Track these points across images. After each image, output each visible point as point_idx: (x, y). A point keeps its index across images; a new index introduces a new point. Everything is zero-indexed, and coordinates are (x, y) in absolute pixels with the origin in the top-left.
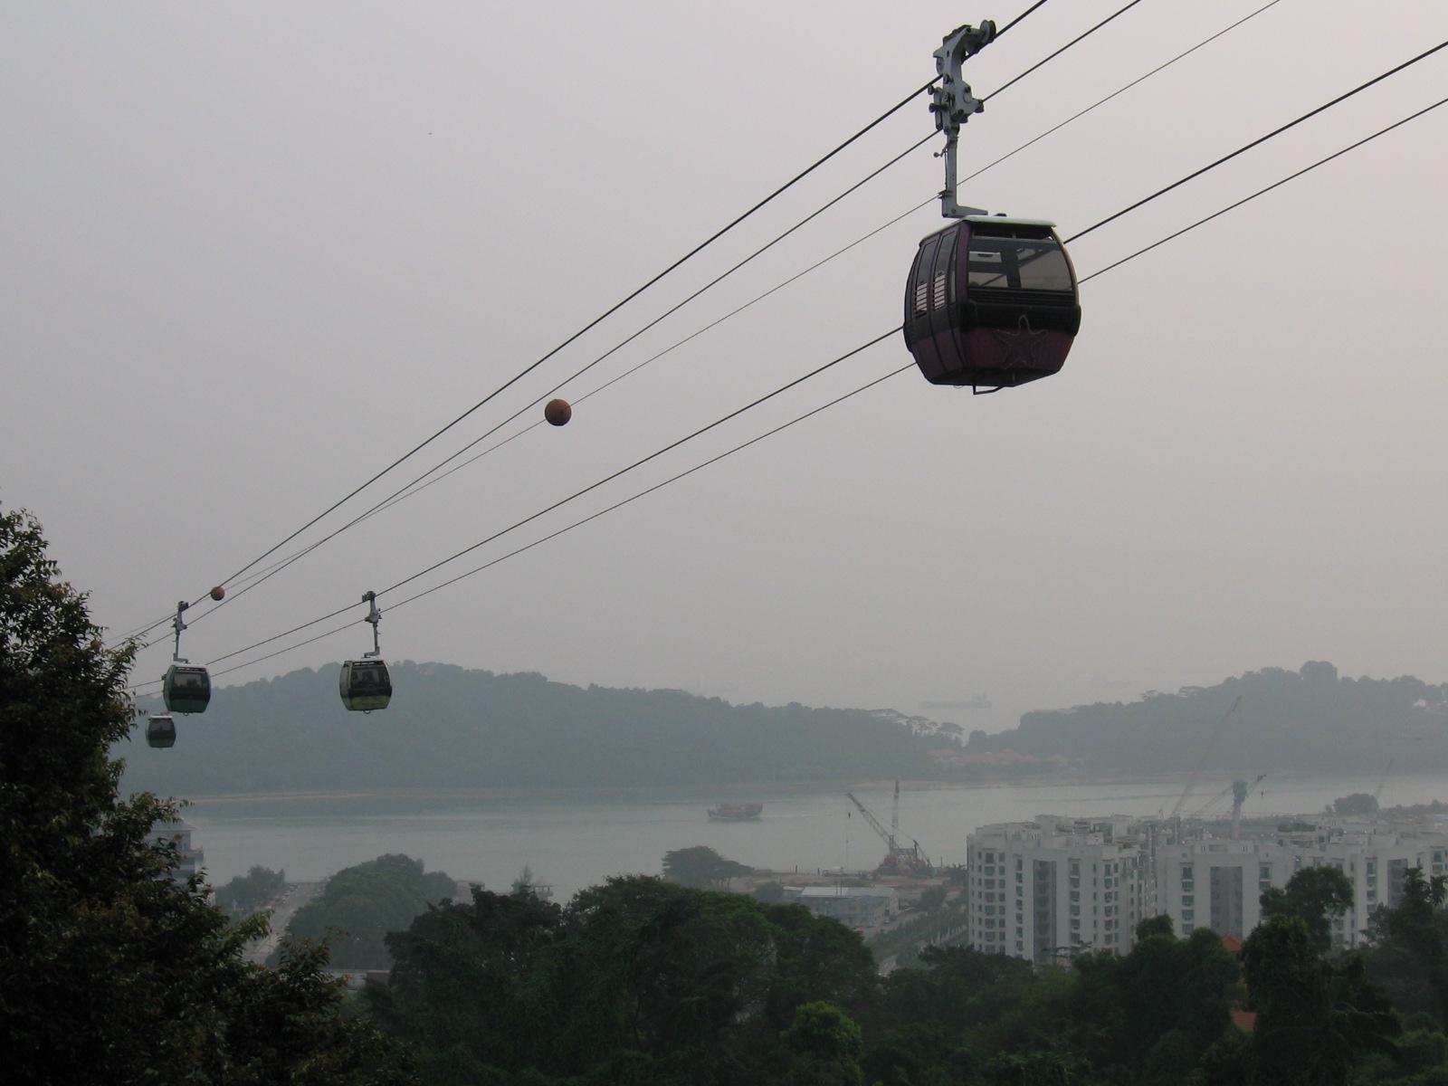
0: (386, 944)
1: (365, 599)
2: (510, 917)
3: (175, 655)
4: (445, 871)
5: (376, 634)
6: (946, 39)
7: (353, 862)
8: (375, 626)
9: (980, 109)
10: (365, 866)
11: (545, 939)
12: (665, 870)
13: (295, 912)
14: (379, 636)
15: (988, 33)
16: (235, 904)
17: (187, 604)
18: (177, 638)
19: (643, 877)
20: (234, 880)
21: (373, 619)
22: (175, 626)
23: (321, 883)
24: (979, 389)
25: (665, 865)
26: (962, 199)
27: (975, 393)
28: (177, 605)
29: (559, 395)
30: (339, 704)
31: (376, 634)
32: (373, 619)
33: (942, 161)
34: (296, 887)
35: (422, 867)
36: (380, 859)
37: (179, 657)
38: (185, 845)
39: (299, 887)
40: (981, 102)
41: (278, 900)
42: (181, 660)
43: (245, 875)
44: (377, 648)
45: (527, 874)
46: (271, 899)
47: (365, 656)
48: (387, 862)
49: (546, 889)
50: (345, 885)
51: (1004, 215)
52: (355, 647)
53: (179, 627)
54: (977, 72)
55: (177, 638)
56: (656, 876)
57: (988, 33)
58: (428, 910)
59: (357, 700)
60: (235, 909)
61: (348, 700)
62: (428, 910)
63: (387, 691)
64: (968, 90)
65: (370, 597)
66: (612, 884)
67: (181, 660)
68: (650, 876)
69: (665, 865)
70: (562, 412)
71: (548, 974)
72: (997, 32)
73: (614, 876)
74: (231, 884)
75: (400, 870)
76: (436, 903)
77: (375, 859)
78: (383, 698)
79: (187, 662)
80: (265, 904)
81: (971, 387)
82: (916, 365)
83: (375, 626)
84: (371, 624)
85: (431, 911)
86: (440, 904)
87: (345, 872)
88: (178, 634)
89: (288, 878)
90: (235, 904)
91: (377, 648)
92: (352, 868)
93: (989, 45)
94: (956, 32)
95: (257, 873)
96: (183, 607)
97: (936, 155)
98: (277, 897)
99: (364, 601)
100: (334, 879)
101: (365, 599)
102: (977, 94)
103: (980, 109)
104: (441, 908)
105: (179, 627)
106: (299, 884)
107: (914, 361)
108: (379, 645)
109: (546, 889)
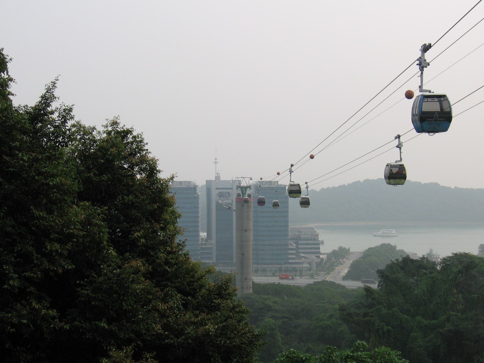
0: (377, 273)
1: (396, 138)
2: (410, 267)
3: (290, 180)
4: (403, 249)
5: (401, 152)
6: (422, 47)
7: (373, 246)
8: (400, 149)
9: (429, 65)
10: (376, 247)
11: (425, 274)
12: (479, 250)
13: (352, 262)
14: (402, 153)
15: (430, 46)
16: (333, 258)
17: (293, 165)
18: (291, 175)
19: (464, 253)
20: (333, 250)
21: (399, 146)
22: (290, 171)
23: (362, 252)
24: (430, 134)
25: (479, 249)
26: (424, 88)
27: (429, 135)
28: (290, 165)
29: (278, 175)
30: (299, 205)
31: (401, 152)
32: (399, 146)
33: (420, 78)
34: (353, 253)
35: (396, 248)
36: (381, 245)
37: (291, 181)
38: (317, 239)
39: (355, 253)
40: (429, 63)
41: (347, 258)
42: (292, 182)
43: (336, 249)
44: (401, 159)
45: (431, 251)
46: (345, 257)
47: (396, 162)
48: (383, 245)
49: (438, 256)
50: (370, 253)
51: (433, 92)
52: (393, 158)
53: (291, 172)
54: (428, 56)
55: (291, 175)
56: (469, 253)
57: (430, 46)
58: (391, 262)
59: (392, 181)
60: (333, 260)
61: (388, 180)
62: (391, 262)
63: (309, 204)
64: (425, 60)
65: (399, 137)
66: (453, 255)
67: (292, 182)
68: (467, 253)
69: (479, 249)
70: (411, 94)
71: (426, 285)
72: (432, 46)
73: (455, 252)
74: (332, 252)
75: (388, 248)
76: (394, 260)
77: (380, 245)
78: (403, 180)
79: (294, 182)
80: (343, 259)
81: (428, 134)
82: (414, 129)
83: (400, 149)
84: (399, 149)
85: (392, 263)
86: (395, 261)
87: (370, 249)
88: (291, 173)
89: (351, 251)
90: (333, 258)
91: (401, 159)
92: (372, 248)
93: (430, 49)
94: (423, 45)
95: (341, 248)
96: (292, 166)
97: (418, 76)
98: (347, 257)
99: (395, 139)
100: (366, 251)
101: (396, 138)
102: (428, 61)
103: (429, 65)
104: (395, 262)
105: (291, 172)
106: (354, 252)
107: (414, 128)
108: (402, 157)
109: (438, 256)
